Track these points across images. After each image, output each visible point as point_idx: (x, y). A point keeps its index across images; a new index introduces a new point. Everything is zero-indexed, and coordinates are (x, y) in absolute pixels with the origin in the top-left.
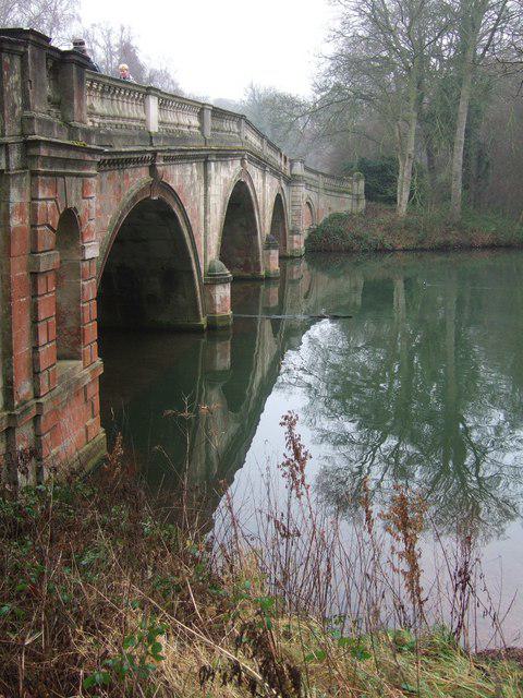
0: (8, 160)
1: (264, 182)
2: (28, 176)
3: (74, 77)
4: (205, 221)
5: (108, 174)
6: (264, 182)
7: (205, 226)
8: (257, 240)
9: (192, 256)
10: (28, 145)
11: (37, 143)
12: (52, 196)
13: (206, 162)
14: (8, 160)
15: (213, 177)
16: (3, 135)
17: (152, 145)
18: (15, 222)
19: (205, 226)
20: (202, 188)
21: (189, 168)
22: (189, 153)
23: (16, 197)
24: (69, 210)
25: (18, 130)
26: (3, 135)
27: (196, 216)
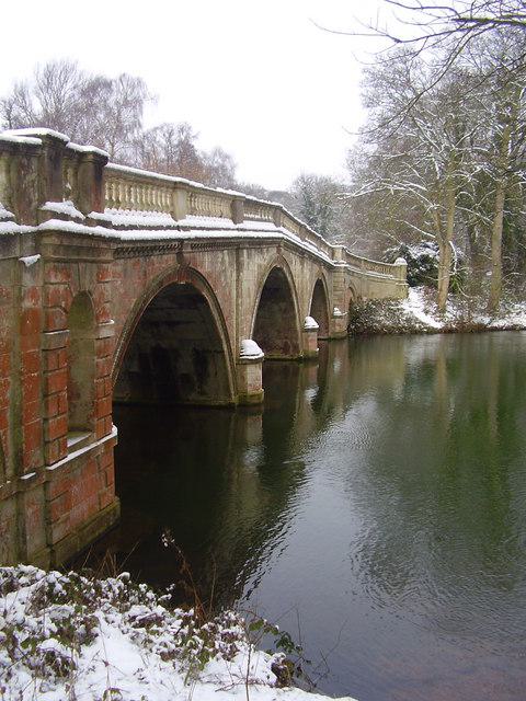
4: (237, 305)
5: (132, 261)
8: (295, 324)
9: (222, 337)
20: (234, 274)
21: (220, 255)
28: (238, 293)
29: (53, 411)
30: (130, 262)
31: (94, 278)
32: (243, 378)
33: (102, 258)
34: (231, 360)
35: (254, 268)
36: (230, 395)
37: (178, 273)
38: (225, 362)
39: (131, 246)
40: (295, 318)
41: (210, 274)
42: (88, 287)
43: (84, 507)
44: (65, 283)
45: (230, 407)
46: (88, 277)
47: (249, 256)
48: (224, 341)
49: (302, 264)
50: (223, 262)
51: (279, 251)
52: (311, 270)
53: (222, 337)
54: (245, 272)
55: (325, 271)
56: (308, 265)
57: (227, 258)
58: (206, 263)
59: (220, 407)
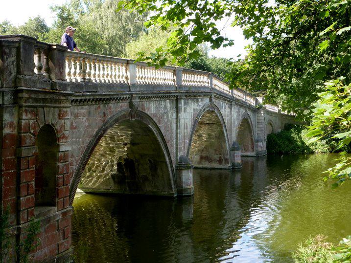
0: (3, 99)
1: (231, 112)
2: (17, 108)
3: (67, 65)
4: (177, 134)
5: (95, 106)
6: (231, 112)
7: (177, 136)
8: (225, 145)
9: (165, 153)
10: (16, 93)
11: (22, 91)
12: (33, 118)
13: (177, 100)
14: (3, 99)
15: (183, 108)
16: (2, 87)
17: (130, 91)
18: (7, 131)
19: (177, 136)
20: (174, 115)
21: (163, 103)
22: (160, 95)
23: (7, 118)
24: (49, 125)
25: (13, 85)
26: (2, 87)
27: (169, 130)
28: (177, 126)
29: (23, 192)
30: (93, 108)
31: (57, 117)
32: (180, 178)
33: (62, 105)
34: (172, 167)
35: (190, 111)
36: (171, 189)
37: (131, 115)
38: (168, 167)
39: (100, 97)
40: (225, 141)
41: (154, 115)
42: (50, 120)
43: (46, 250)
44: (33, 119)
45: (170, 198)
46: (51, 115)
47: (186, 104)
48: (227, 141)
49: (231, 108)
50: (165, 107)
51: (211, 100)
52: (238, 112)
53: (165, 153)
54: (182, 113)
55: (249, 112)
56: (235, 109)
57: (168, 105)
58: (152, 108)
59: (164, 197)
